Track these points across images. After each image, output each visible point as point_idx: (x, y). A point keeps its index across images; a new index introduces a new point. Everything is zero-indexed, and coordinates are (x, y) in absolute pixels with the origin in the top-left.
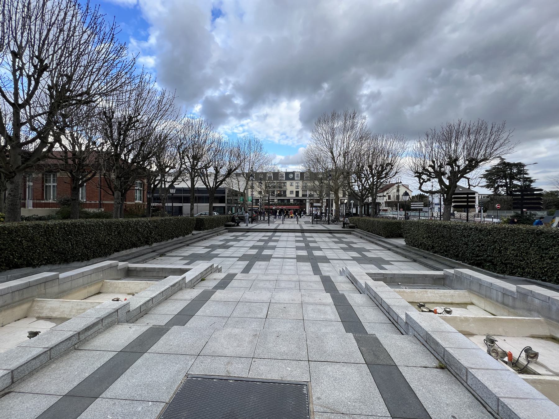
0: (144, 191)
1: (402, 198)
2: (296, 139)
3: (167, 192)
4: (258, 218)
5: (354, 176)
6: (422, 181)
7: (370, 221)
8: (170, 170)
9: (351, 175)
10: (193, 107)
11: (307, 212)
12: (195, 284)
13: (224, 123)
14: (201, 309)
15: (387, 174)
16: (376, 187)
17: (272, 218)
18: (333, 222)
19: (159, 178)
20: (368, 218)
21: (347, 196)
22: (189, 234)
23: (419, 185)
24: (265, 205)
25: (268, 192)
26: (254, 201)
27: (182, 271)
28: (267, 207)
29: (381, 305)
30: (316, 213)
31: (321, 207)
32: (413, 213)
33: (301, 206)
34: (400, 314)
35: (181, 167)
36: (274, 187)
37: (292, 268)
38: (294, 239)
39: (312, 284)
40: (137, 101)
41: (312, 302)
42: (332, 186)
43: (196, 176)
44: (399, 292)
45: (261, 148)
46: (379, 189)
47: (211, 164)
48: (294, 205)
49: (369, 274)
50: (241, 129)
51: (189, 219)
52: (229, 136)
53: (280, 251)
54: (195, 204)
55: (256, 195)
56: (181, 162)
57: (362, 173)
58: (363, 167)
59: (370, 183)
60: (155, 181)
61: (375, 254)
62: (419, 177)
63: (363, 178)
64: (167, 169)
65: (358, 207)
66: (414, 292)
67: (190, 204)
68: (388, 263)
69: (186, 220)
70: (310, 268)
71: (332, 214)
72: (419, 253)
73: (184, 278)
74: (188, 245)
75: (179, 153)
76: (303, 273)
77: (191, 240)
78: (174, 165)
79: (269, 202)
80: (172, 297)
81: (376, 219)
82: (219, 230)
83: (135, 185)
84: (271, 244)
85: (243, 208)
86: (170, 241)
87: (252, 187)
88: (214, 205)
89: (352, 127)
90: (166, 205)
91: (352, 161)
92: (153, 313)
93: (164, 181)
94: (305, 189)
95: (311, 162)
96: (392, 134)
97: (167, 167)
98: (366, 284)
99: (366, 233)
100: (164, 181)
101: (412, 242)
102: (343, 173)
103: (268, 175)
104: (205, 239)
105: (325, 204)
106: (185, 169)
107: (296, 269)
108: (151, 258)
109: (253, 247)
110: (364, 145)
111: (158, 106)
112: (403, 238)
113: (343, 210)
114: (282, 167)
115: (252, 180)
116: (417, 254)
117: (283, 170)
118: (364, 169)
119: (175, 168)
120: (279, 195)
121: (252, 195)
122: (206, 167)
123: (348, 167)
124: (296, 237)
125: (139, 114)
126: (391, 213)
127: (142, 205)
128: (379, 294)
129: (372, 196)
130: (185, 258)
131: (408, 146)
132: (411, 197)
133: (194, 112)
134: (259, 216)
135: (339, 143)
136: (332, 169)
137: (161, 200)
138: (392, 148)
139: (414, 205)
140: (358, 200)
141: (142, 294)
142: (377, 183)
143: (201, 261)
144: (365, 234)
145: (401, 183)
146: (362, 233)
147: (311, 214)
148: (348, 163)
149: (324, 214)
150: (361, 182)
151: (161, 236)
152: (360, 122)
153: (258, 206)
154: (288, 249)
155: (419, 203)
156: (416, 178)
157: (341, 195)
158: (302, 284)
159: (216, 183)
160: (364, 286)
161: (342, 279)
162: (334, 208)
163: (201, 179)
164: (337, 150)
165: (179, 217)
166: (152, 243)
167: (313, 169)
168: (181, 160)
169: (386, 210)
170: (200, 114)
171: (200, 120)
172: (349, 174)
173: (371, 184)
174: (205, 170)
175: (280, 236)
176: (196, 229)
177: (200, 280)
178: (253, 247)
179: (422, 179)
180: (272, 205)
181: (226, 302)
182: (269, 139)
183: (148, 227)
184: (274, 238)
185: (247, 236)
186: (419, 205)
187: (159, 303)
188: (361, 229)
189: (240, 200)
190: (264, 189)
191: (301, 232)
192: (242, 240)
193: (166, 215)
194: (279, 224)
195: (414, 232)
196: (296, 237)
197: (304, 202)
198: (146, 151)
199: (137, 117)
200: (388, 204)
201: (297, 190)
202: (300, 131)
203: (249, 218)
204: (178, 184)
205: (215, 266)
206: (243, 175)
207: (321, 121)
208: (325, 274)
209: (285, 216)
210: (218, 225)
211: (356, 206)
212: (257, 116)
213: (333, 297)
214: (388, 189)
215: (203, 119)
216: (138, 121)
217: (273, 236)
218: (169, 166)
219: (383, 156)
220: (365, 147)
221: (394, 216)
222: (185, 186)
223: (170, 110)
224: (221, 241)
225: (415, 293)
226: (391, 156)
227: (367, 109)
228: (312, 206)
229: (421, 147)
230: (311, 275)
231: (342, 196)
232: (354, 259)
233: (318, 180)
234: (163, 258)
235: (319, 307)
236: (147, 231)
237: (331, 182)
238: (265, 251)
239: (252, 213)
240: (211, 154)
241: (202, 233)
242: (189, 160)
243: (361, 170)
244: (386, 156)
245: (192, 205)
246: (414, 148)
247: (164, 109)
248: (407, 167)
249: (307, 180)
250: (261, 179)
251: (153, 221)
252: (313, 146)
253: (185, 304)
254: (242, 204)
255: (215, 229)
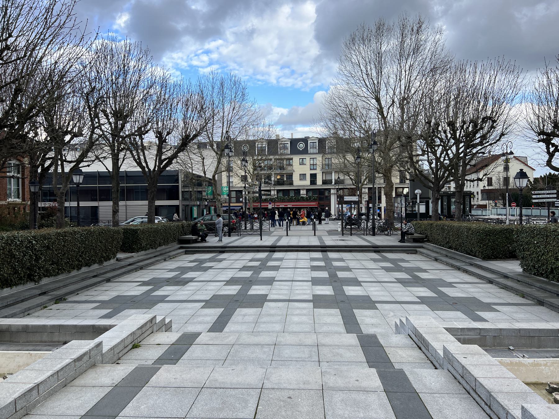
0: (23, 179)
1: (514, 183)
2: (310, 74)
3: (67, 180)
4: (240, 226)
5: (420, 142)
6: (552, 149)
7: (452, 227)
8: (72, 139)
9: (415, 141)
10: (114, 18)
11: (333, 212)
12: (120, 355)
13: (173, 48)
14: (130, 405)
15: (484, 137)
16: (464, 162)
17: (266, 225)
18: (383, 231)
19: (51, 154)
20: (447, 222)
21: (408, 182)
22: (110, 259)
23: (547, 157)
24: (254, 201)
25: (258, 177)
26: (233, 194)
27: (98, 331)
28: (258, 205)
29: (475, 391)
30: (349, 214)
31: (358, 203)
32: (536, 212)
33: (322, 202)
34: (511, 407)
35: (93, 132)
36: (270, 168)
37: (304, 319)
38: (307, 264)
39: (341, 351)
40: (6, 10)
41: (342, 385)
42: (380, 164)
43: (123, 149)
44: (510, 367)
45: (243, 95)
46: (468, 167)
47: (149, 127)
48: (308, 200)
49: (450, 330)
50: (205, 58)
51: (109, 231)
52: (183, 71)
53: (282, 287)
54: (121, 203)
55: (237, 183)
56: (93, 124)
57: (437, 137)
58: (437, 125)
59: (451, 156)
60: (44, 160)
61: (463, 291)
62: (547, 142)
63: (439, 146)
64: (67, 138)
65: (430, 201)
66: (538, 365)
67: (111, 203)
68: (489, 307)
69: (102, 232)
70: (339, 319)
71: (380, 215)
72: (549, 287)
73: (100, 345)
74: (108, 280)
75: (89, 107)
76: (325, 329)
77: (114, 270)
78: (80, 130)
79: (260, 195)
80: (77, 382)
81: (465, 224)
82: (168, 250)
83: (8, 169)
84: (265, 274)
85: (213, 208)
86: (74, 273)
87: (229, 169)
88: (158, 203)
89: (416, 50)
90: (67, 204)
91: (416, 115)
92: (39, 412)
93: (61, 159)
94: (327, 169)
95: (338, 119)
96: (493, 62)
97: (67, 133)
98: (445, 350)
99: (444, 250)
100: (61, 159)
101: (534, 267)
102: (399, 138)
103: (259, 145)
104: (141, 268)
105: (366, 198)
106: (100, 136)
107: (312, 322)
108: (38, 306)
109: (231, 282)
110: (439, 84)
111: (46, 18)
112: (518, 260)
113: (401, 207)
114: (284, 129)
115: (228, 155)
116: (545, 290)
117: (286, 135)
118: (440, 129)
119: (81, 135)
120: (279, 182)
121: (229, 182)
122: (141, 133)
123: (409, 125)
124: (312, 259)
125: (10, 36)
126: (494, 211)
127: (22, 207)
128: (471, 369)
129: (456, 180)
130: (103, 304)
131: (524, 82)
132: (532, 180)
133: (115, 27)
134: (243, 223)
135: (392, 81)
136: (379, 131)
137: (55, 196)
138: (493, 87)
139: (538, 196)
140: (430, 188)
141: (19, 377)
142: (466, 155)
143: (133, 311)
144: (444, 252)
145: (511, 153)
146: (438, 250)
147: (341, 216)
148: (409, 118)
149: (364, 217)
150: (434, 153)
151: (57, 263)
152: (431, 38)
153: (241, 204)
154: (298, 283)
155: (548, 192)
156: (541, 143)
157: (396, 180)
158: (324, 351)
159: (161, 163)
160: (441, 353)
161: (400, 339)
162: (383, 204)
163: (132, 154)
164: (387, 93)
165: (92, 227)
166: (40, 278)
167: (342, 132)
168: (92, 120)
169: (484, 207)
170: (126, 32)
171: (126, 44)
172: (410, 139)
173: (453, 158)
174: (138, 138)
175: (281, 259)
176: (124, 250)
177: (130, 347)
178: (231, 282)
179: (553, 145)
180: (266, 201)
181: (179, 389)
182: (259, 77)
183: (32, 248)
184: (270, 264)
185: (221, 260)
186: (548, 196)
187: (52, 393)
188: (436, 244)
189: (207, 192)
190: (251, 171)
191: (322, 251)
192: (211, 268)
193: (66, 224)
194: (281, 237)
195: (539, 247)
196: (312, 259)
197: (326, 194)
198: (26, 104)
199: (6, 40)
200: (488, 194)
201: (313, 172)
202: (317, 60)
203: (224, 225)
204: (88, 166)
205: (159, 319)
206: (212, 146)
207: (357, 39)
208: (367, 330)
209: (291, 221)
210: (166, 242)
211: (425, 200)
212: (235, 34)
213: (382, 376)
214: (487, 166)
215: (133, 41)
216: (7, 48)
217: (268, 259)
218: (70, 132)
219: (476, 103)
220: (441, 86)
221: (500, 217)
222: (102, 169)
223: (69, 24)
224: (171, 270)
225: (541, 365)
226: (490, 102)
227: (445, 12)
228: (341, 201)
229: (550, 84)
230: (340, 333)
231: (398, 181)
232: (423, 300)
233: (351, 152)
234: (61, 305)
235: (354, 395)
236: (30, 256)
237: (376, 155)
238: (254, 287)
239: (229, 216)
240: (149, 107)
241: (136, 256)
242: (108, 119)
243: (433, 132)
244: (482, 104)
245: (116, 204)
246: (537, 86)
247: (56, 24)
248: (523, 123)
249: (331, 153)
250: (245, 154)
251: (41, 236)
252: (342, 87)
253: (101, 394)
254: (211, 201)
255: (159, 249)
